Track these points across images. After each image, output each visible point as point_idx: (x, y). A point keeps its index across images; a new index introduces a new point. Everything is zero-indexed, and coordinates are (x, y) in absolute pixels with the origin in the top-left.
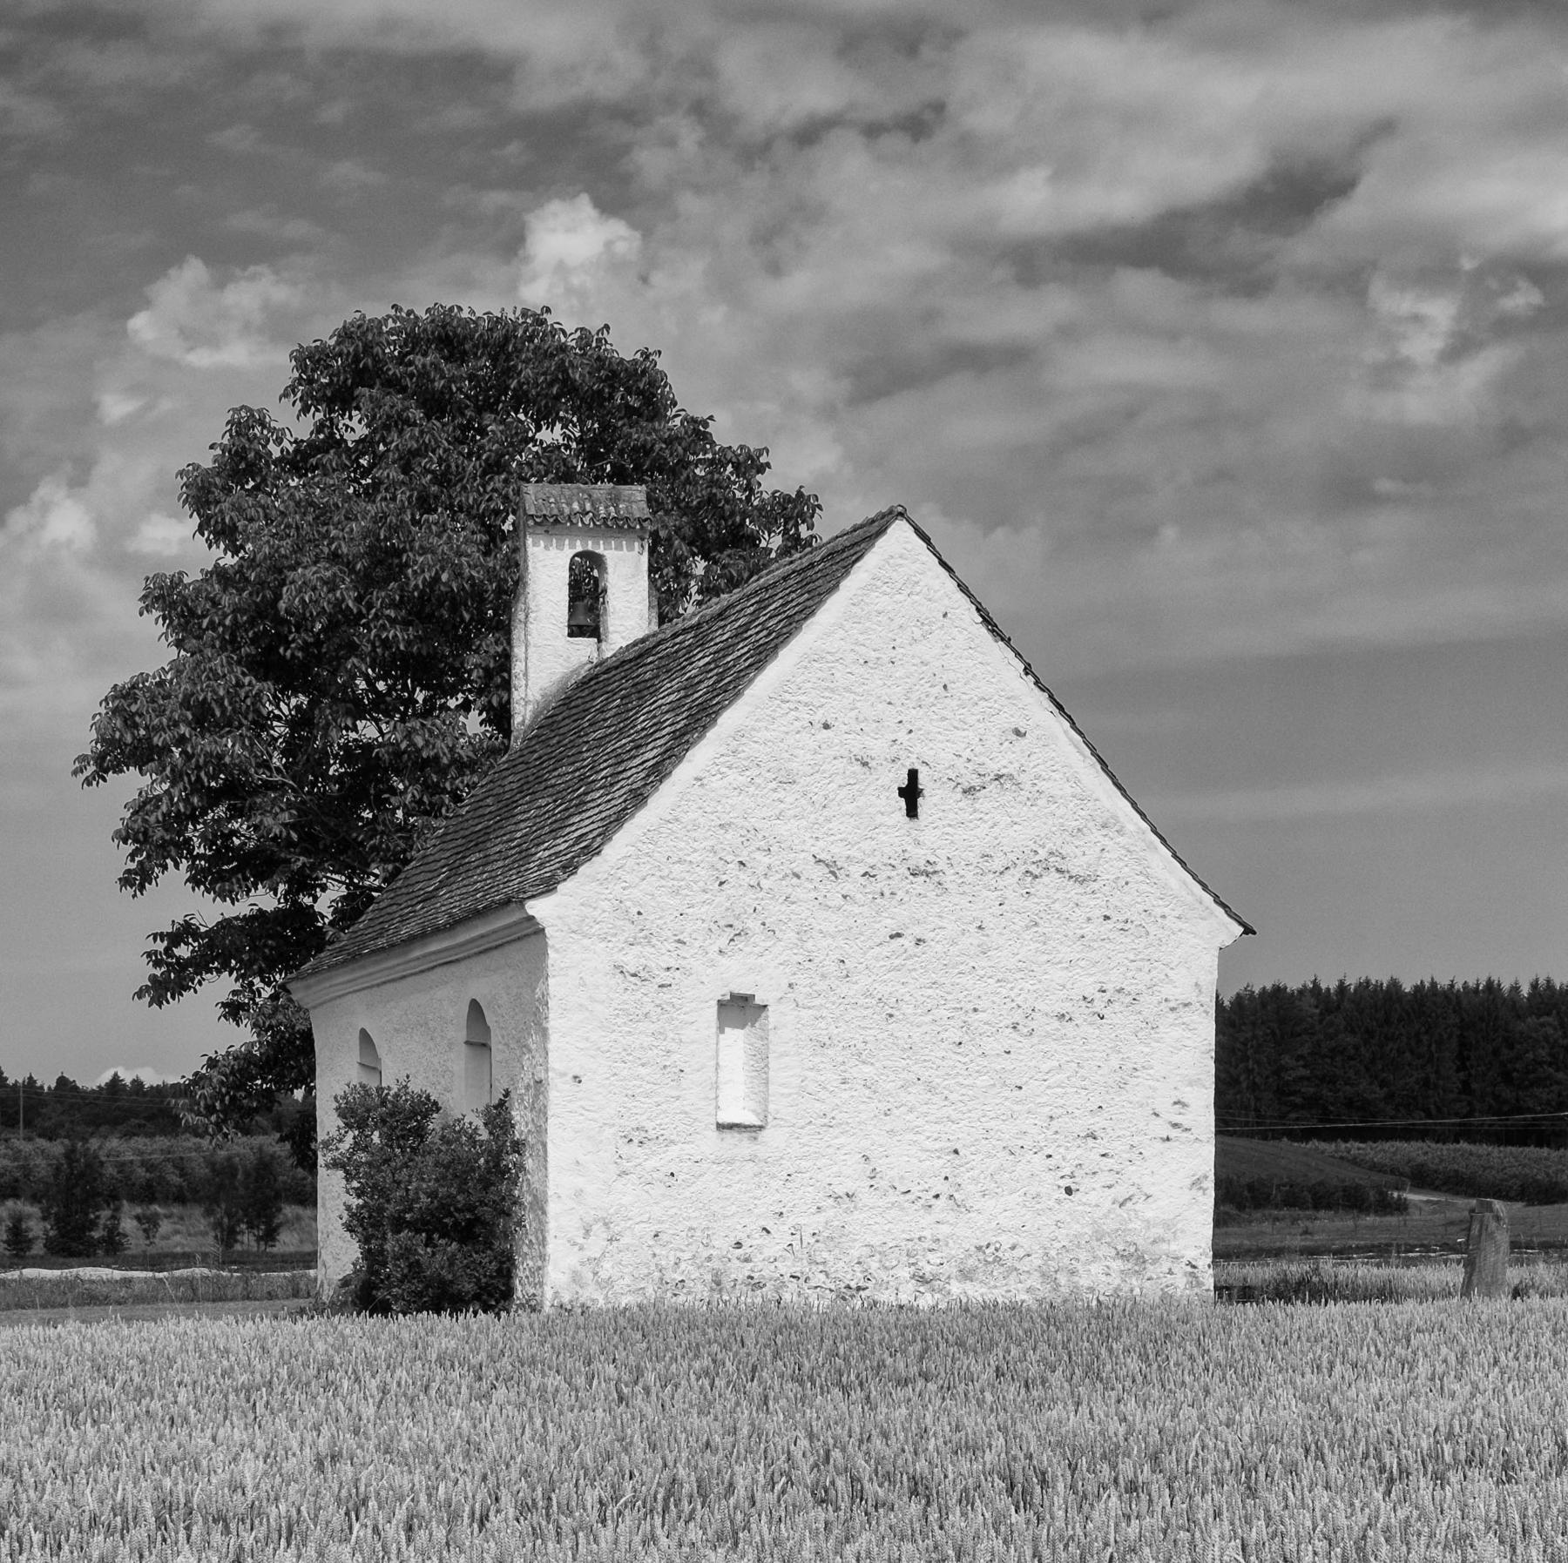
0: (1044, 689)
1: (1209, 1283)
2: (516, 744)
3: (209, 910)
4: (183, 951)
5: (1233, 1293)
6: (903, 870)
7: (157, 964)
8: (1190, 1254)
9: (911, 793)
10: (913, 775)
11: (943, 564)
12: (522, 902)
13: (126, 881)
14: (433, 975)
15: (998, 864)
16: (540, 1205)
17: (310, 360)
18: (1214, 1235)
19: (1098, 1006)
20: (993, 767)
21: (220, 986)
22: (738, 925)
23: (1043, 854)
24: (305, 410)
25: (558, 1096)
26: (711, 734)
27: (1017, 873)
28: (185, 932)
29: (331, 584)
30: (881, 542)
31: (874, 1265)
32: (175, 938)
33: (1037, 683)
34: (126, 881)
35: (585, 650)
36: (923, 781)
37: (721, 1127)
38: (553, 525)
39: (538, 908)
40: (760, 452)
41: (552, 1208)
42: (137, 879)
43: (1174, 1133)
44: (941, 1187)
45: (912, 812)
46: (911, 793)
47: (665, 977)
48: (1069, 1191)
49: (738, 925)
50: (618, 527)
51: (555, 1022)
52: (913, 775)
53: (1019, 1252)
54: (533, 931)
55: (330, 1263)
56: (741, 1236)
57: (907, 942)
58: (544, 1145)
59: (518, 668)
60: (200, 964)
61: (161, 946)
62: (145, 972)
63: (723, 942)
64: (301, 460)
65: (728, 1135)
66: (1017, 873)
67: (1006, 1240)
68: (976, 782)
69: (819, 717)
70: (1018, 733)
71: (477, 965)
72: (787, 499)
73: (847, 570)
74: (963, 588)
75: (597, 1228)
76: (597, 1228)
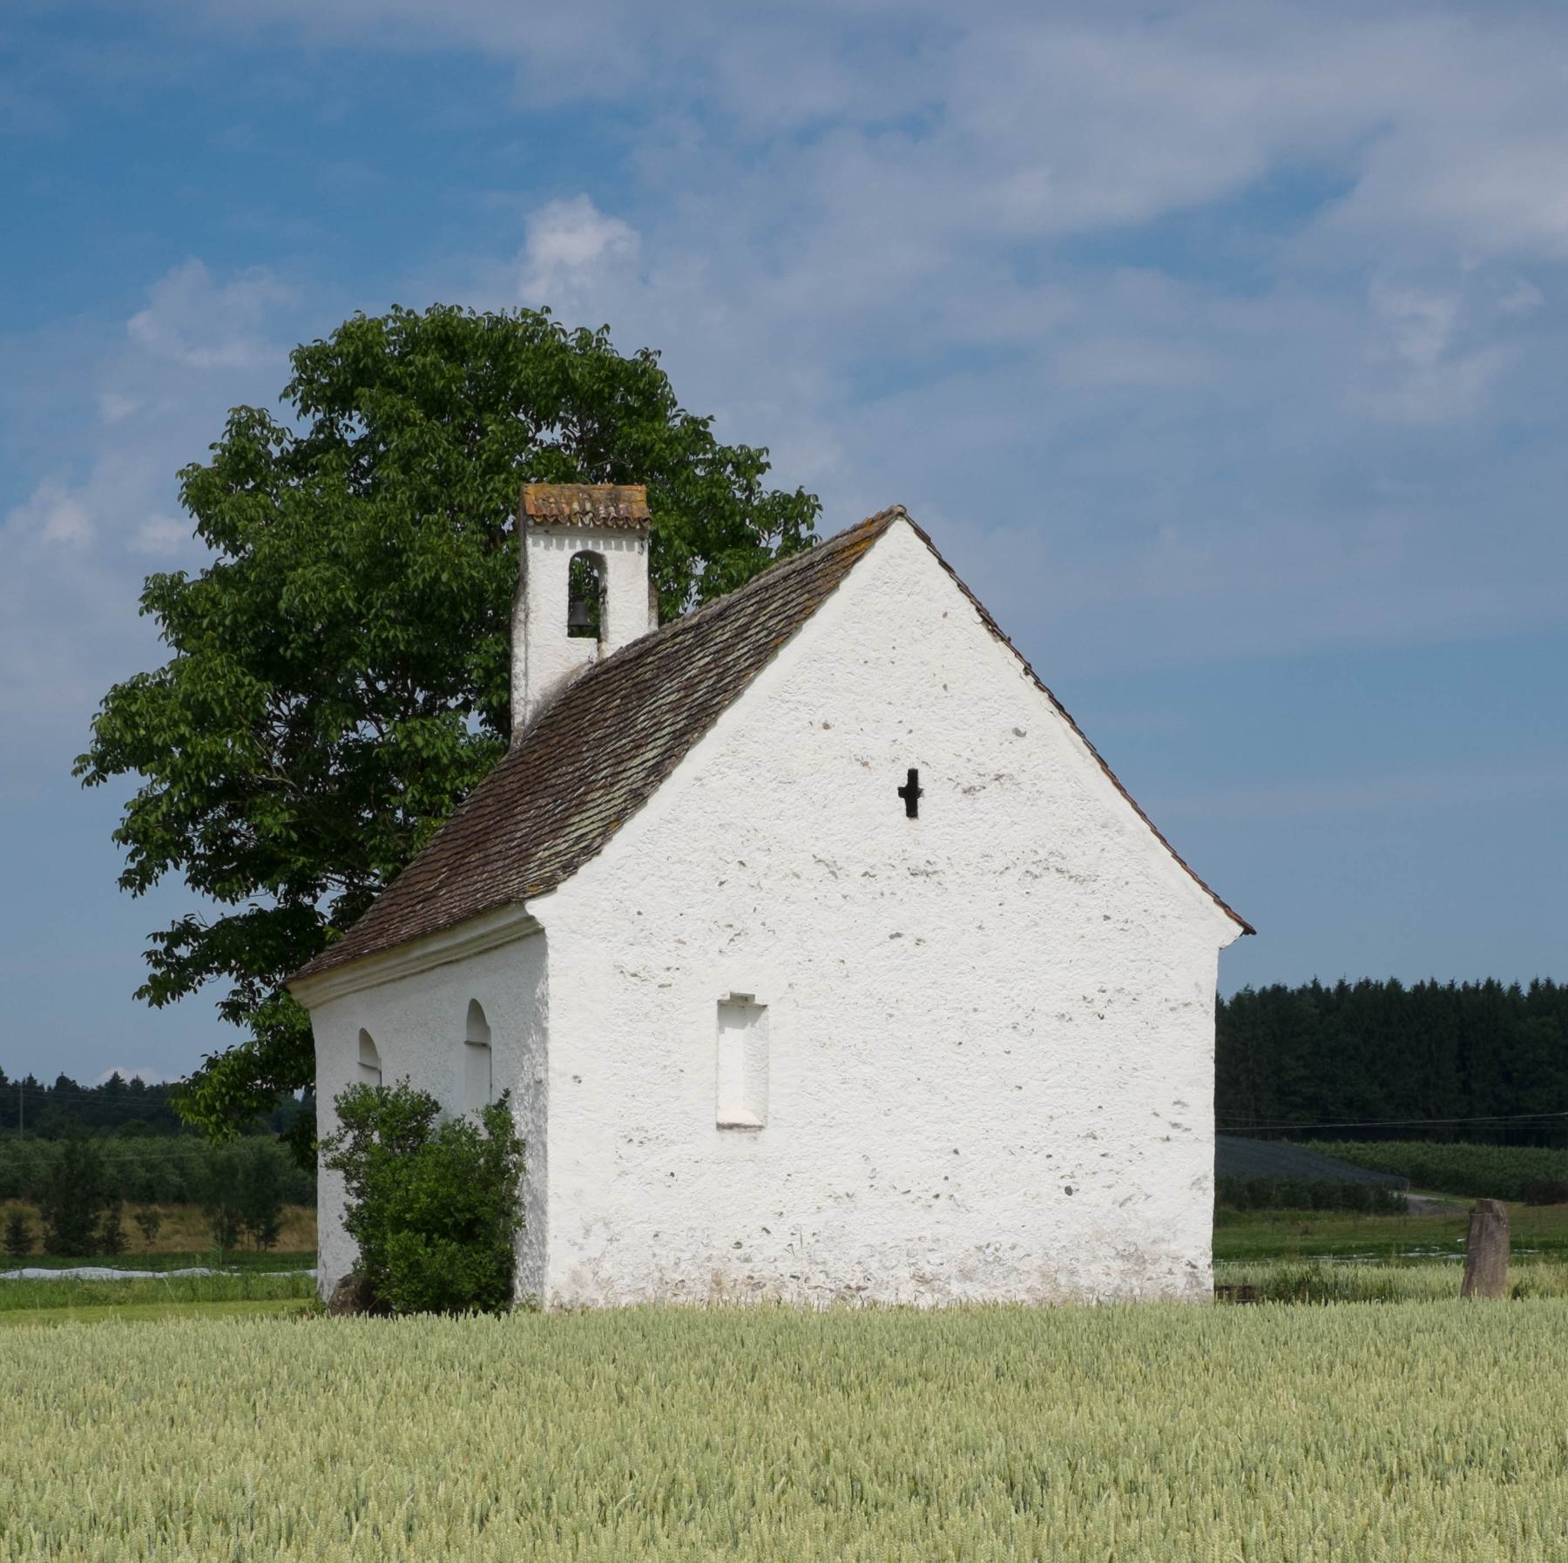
0: (1043, 689)
1: (1210, 1283)
2: (516, 744)
3: (209, 910)
4: (183, 951)
6: (902, 870)
7: (157, 964)
8: (1190, 1254)
9: (911, 793)
11: (943, 564)
12: (521, 902)
13: (126, 881)
15: (998, 864)
16: (540, 1206)
17: (310, 360)
18: (1214, 1235)
19: (1099, 1006)
20: (993, 768)
21: (220, 986)
22: (738, 926)
23: (1043, 854)
24: (305, 410)
25: (558, 1096)
26: (711, 734)
28: (185, 932)
29: (331, 585)
31: (873, 1265)
32: (176, 937)
33: (1037, 683)
34: (126, 881)
36: (923, 782)
37: (721, 1127)
38: (553, 525)
40: (761, 452)
43: (1173, 1133)
44: (941, 1188)
45: (912, 811)
46: (911, 793)
47: (665, 977)
48: (1069, 1191)
49: (738, 926)
50: (618, 528)
53: (1019, 1252)
55: (330, 1263)
56: (740, 1236)
57: (907, 942)
58: (544, 1145)
61: (160, 946)
62: (144, 972)
64: (301, 460)
65: (727, 1134)
67: (1006, 1240)
68: (976, 782)
69: (819, 718)
70: (1018, 733)
72: (788, 498)
73: (847, 570)
74: (963, 588)
75: (598, 1228)
76: (598, 1228)
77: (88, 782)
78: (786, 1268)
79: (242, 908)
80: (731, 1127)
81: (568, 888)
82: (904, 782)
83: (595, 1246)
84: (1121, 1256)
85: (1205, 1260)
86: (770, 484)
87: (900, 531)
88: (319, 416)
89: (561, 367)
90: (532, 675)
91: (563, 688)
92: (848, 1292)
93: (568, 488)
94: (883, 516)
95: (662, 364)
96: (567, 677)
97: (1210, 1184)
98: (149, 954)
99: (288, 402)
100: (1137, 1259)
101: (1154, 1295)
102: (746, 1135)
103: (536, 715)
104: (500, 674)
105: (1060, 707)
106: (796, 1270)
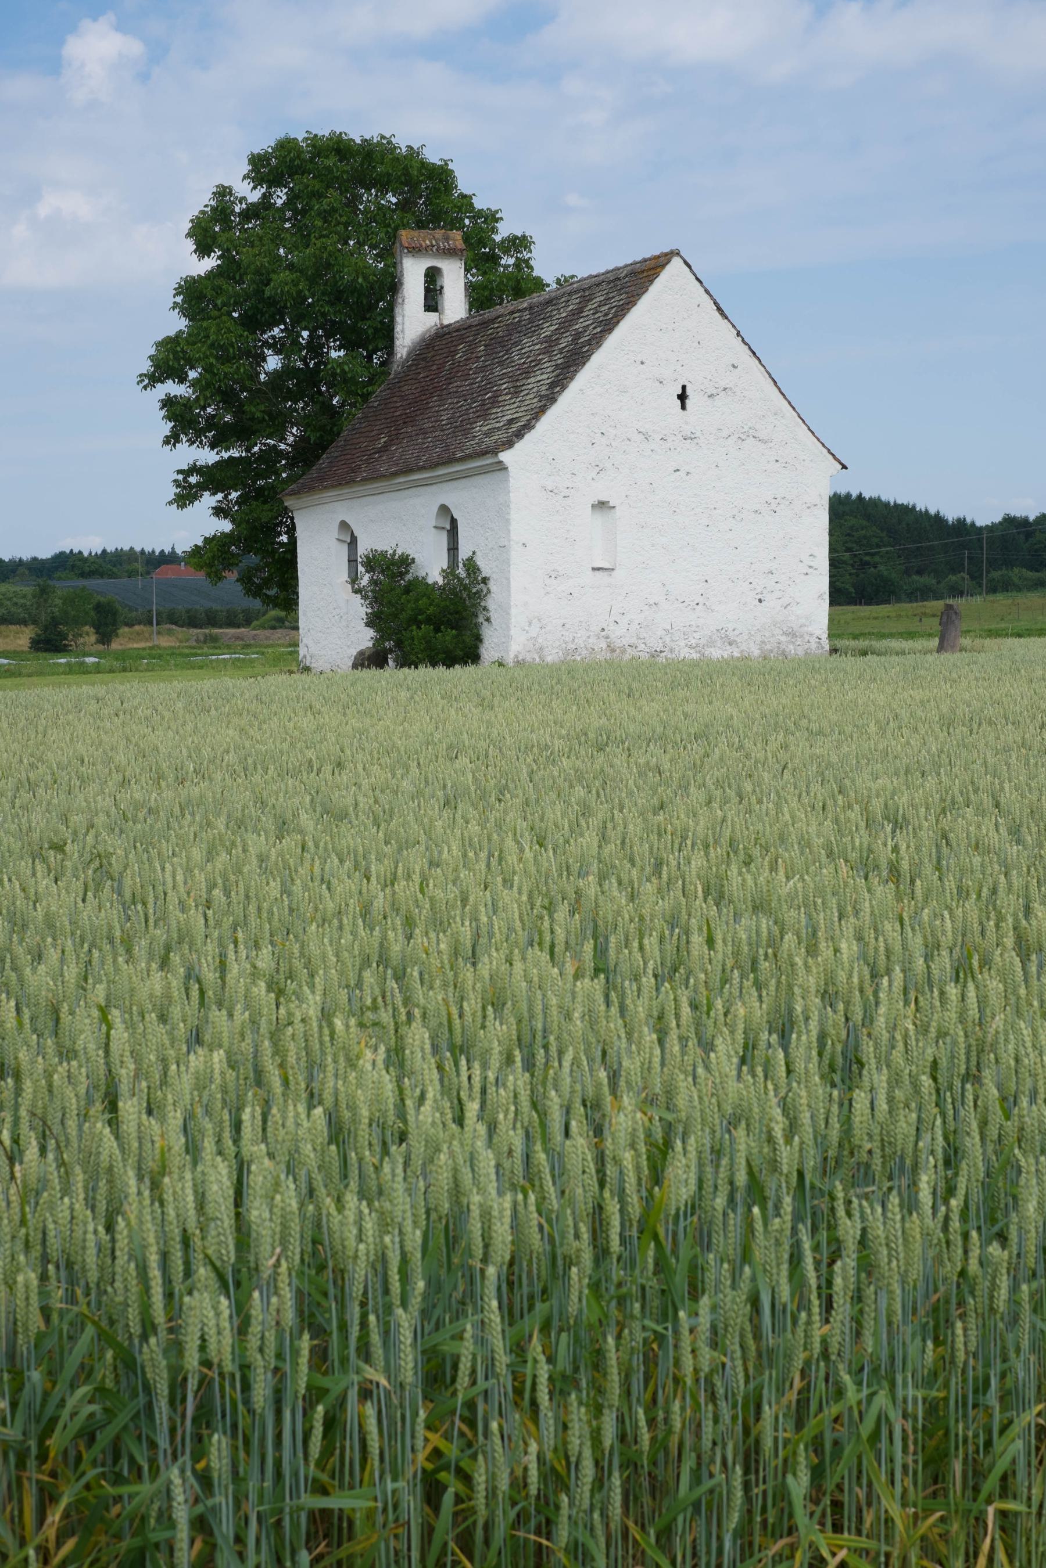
0: (746, 344)
1: (827, 647)
2: (395, 368)
3: (208, 456)
4: (193, 479)
5: (834, 651)
6: (679, 437)
7: (178, 486)
8: (818, 633)
9: (682, 397)
10: (684, 388)
11: (698, 279)
12: (496, 454)
13: (166, 442)
14: (407, 492)
15: (725, 433)
16: (506, 610)
17: (257, 161)
18: (831, 620)
19: (773, 506)
20: (723, 384)
21: (209, 500)
22: (601, 466)
23: (746, 428)
24: (255, 188)
25: (516, 554)
26: (588, 365)
27: (734, 438)
28: (193, 469)
29: (294, 282)
30: (668, 267)
31: (668, 639)
32: (187, 473)
33: (743, 341)
34: (166, 442)
35: (432, 318)
36: (689, 391)
37: (594, 569)
38: (416, 251)
39: (505, 456)
40: (497, 212)
41: (513, 611)
42: (172, 440)
43: (810, 571)
44: (701, 600)
45: (683, 407)
46: (682, 397)
47: (566, 492)
48: (760, 601)
49: (601, 466)
50: (450, 253)
51: (514, 516)
52: (684, 388)
53: (737, 632)
54: (501, 467)
55: (311, 644)
56: (605, 626)
57: (682, 473)
58: (508, 579)
59: (398, 328)
60: (202, 487)
61: (180, 477)
62: (172, 491)
63: (594, 474)
64: (252, 212)
65: (597, 573)
66: (734, 438)
67: (731, 626)
68: (714, 392)
69: (639, 359)
70: (734, 366)
71: (445, 486)
72: (516, 238)
73: (651, 282)
74: (707, 291)
75: (535, 621)
76: (535, 621)
77: (145, 388)
78: (625, 642)
79: (226, 455)
80: (599, 569)
81: (520, 446)
82: (680, 392)
83: (534, 631)
84: (785, 634)
85: (825, 636)
86: (504, 231)
87: (676, 262)
88: (263, 190)
89: (406, 168)
90: (407, 332)
91: (423, 339)
92: (655, 654)
93: (423, 232)
94: (666, 254)
95: (451, 166)
96: (424, 334)
97: (827, 597)
98: (175, 481)
99: (246, 182)
100: (792, 634)
101: (801, 652)
102: (606, 573)
103: (409, 354)
104: (387, 333)
105: (754, 353)
106: (630, 642)
